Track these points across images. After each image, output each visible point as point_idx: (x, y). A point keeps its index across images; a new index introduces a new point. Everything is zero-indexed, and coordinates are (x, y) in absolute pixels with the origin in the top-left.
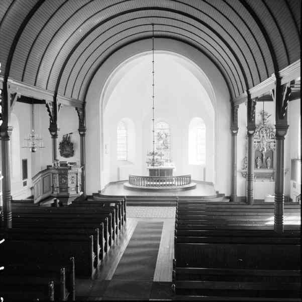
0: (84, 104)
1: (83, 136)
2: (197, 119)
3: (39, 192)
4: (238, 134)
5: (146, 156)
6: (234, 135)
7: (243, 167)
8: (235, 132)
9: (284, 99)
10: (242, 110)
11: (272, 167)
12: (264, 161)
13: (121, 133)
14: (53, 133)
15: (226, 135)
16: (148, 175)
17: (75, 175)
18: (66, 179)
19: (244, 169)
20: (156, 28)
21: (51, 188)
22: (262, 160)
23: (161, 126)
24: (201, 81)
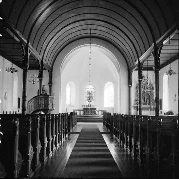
0: (52, 70)
1: (50, 87)
2: (109, 83)
3: (32, 108)
4: (132, 87)
5: (87, 95)
6: (130, 87)
7: (134, 104)
8: (130, 85)
9: (158, 53)
10: (135, 74)
11: (149, 104)
12: (145, 101)
13: (68, 89)
14: (41, 79)
15: (125, 87)
16: (83, 109)
17: (52, 99)
18: (48, 100)
19: (135, 105)
20: (92, 31)
21: (39, 106)
22: (144, 100)
23: (89, 88)
24: (111, 59)
